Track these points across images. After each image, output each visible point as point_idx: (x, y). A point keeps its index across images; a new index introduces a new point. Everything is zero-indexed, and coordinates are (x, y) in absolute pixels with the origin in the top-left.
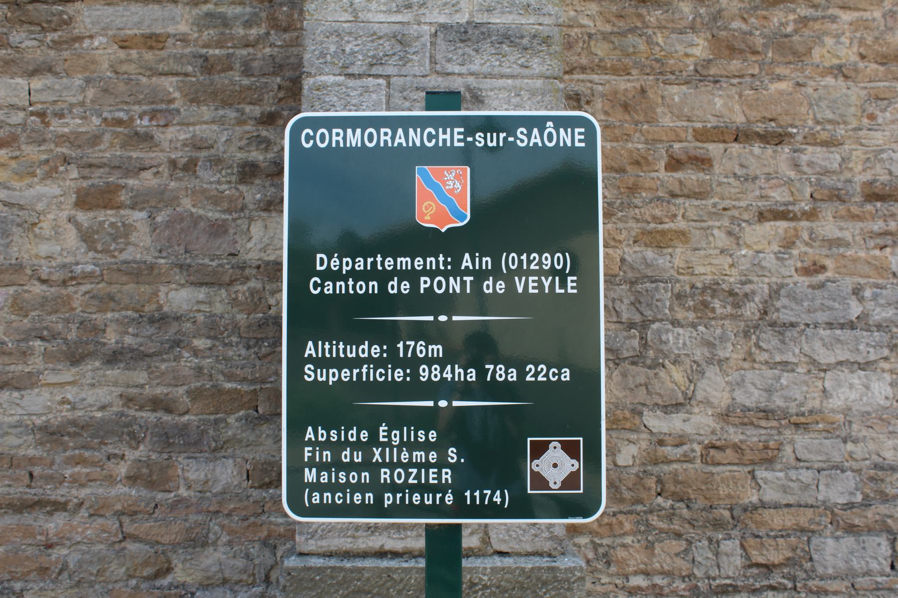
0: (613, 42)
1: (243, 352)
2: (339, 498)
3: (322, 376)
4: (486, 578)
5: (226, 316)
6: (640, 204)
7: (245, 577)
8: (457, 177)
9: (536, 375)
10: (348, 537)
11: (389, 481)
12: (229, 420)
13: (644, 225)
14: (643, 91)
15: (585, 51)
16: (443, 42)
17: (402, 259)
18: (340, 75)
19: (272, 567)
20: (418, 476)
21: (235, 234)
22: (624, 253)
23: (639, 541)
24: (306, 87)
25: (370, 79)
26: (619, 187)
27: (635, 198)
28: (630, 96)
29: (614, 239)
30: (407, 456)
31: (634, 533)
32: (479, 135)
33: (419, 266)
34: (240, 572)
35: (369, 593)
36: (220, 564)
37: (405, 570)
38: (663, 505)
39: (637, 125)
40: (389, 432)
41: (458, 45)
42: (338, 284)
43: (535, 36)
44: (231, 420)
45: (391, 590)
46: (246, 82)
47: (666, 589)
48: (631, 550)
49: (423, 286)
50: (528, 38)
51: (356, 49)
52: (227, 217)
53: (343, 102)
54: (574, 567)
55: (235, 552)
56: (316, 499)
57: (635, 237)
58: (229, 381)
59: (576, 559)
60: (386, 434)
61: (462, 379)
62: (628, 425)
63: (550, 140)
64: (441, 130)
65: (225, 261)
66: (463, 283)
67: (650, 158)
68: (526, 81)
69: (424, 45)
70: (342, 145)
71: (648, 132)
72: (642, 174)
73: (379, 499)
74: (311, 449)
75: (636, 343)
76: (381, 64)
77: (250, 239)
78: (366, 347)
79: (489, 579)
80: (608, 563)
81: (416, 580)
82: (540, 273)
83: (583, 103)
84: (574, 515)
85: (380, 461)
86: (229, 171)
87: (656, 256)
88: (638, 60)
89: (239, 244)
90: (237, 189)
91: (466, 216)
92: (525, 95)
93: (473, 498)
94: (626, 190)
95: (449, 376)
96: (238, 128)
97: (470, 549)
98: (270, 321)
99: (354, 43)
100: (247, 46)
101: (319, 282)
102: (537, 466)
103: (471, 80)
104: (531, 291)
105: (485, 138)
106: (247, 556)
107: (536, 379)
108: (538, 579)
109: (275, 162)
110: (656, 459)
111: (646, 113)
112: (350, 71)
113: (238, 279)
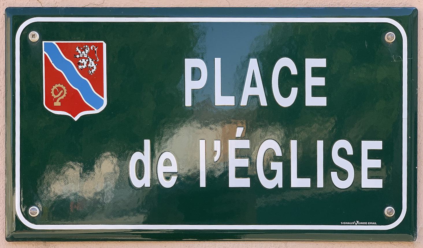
8: (91, 54)
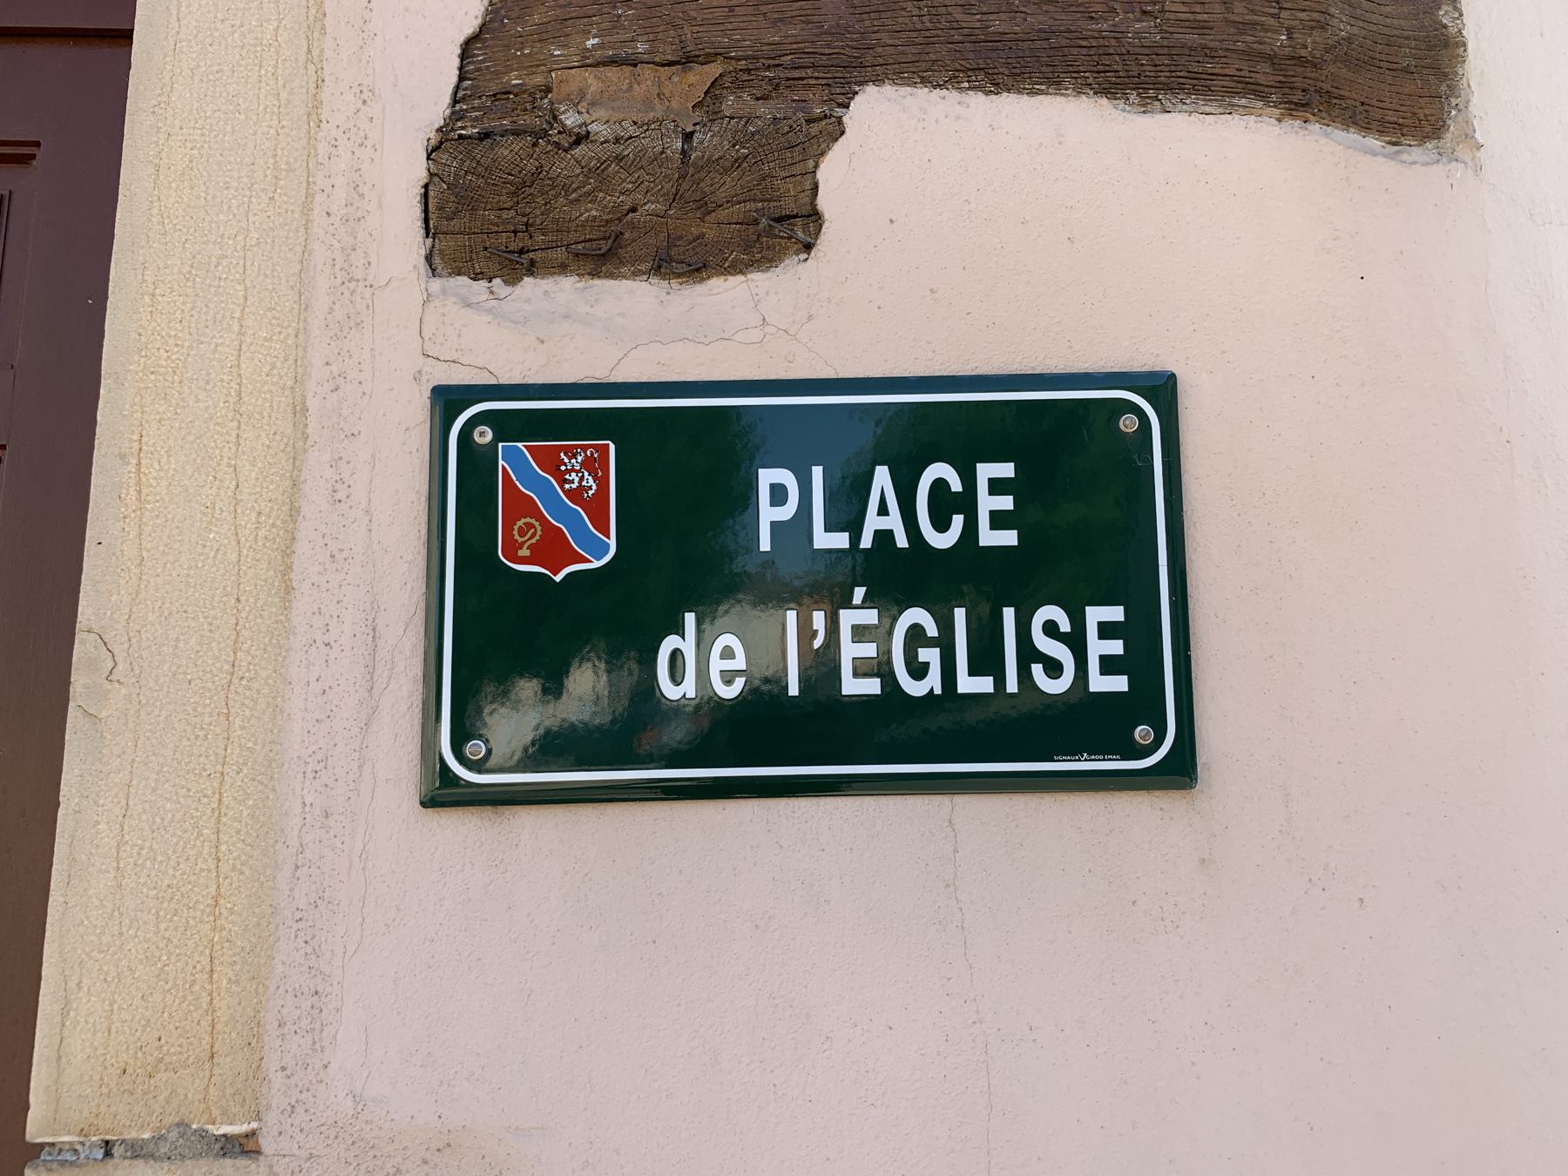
8: (588, 464)
49: (768, 515)
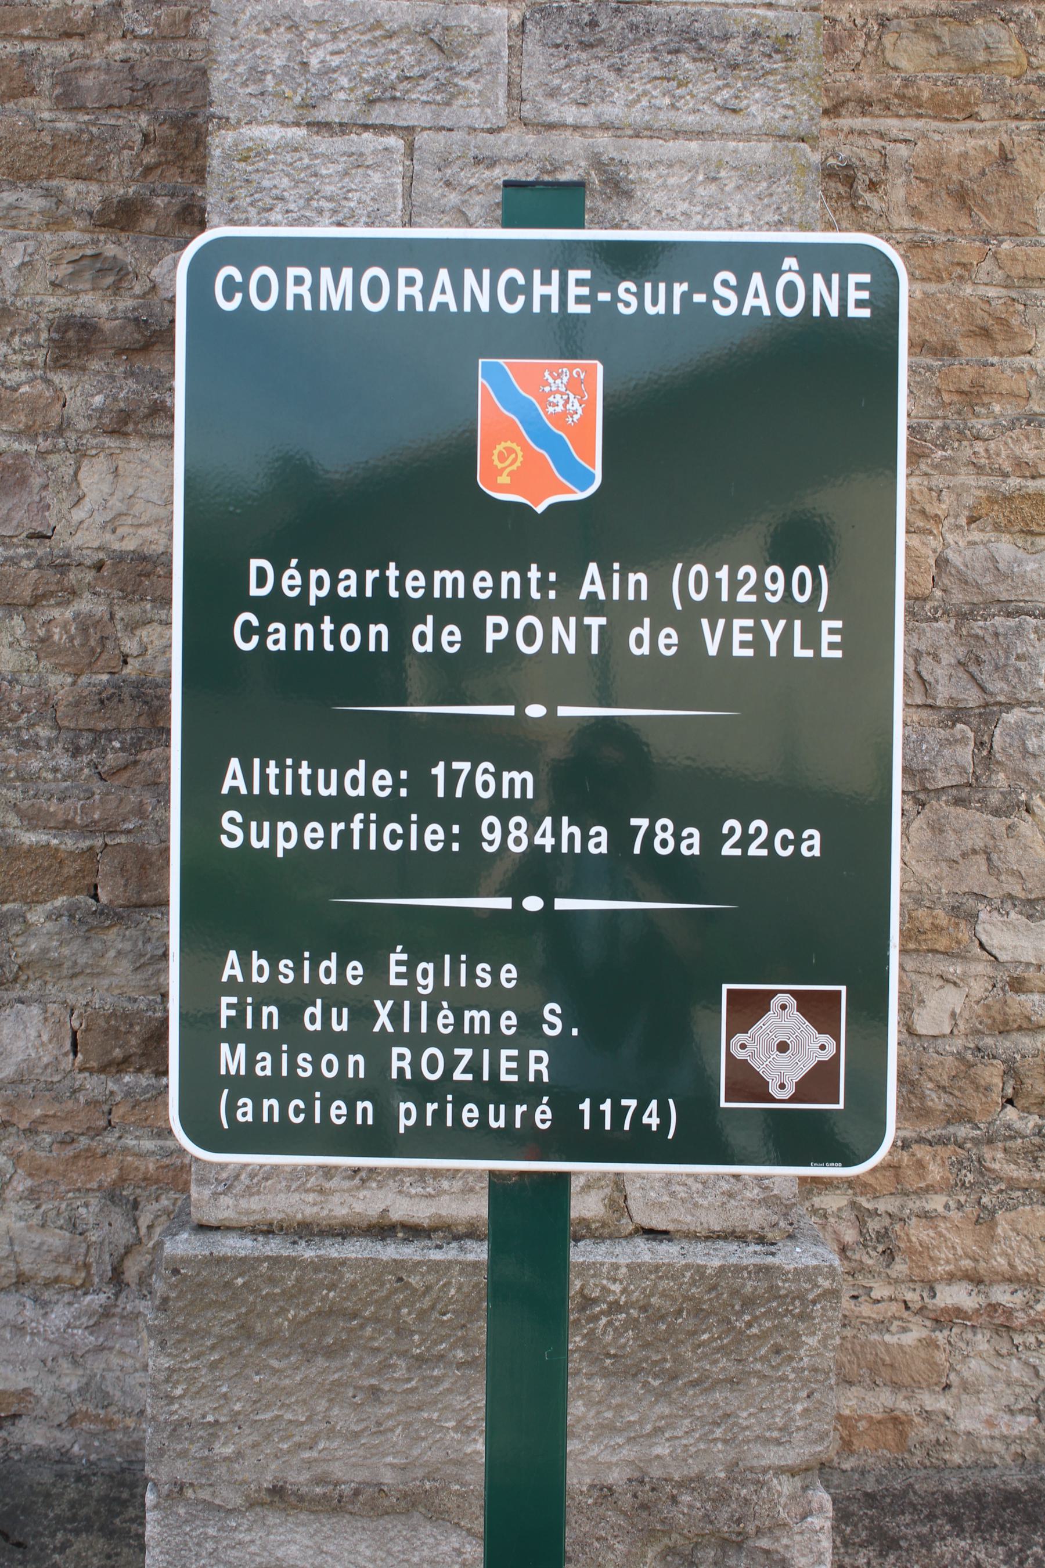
0: (937, 38)
1: (64, 762)
2: (297, 1111)
3: (260, 838)
4: (616, 1288)
5: (25, 678)
6: (987, 432)
7: (66, 1271)
8: (573, 385)
9: (745, 842)
10: (307, 1191)
11: (408, 1076)
12: (32, 917)
13: (996, 480)
14: (1005, 158)
15: (871, 61)
16: (539, 48)
17: (446, 573)
18: (297, 124)
19: (128, 1250)
20: (474, 1067)
21: (45, 487)
22: (946, 545)
23: (960, 1206)
24: (217, 152)
25: (365, 135)
26: (939, 391)
27: (977, 416)
28: (974, 172)
29: (923, 512)
30: (451, 1020)
31: (948, 1188)
32: (626, 288)
33: (483, 590)
34: (55, 1260)
35: (355, 1316)
36: (11, 1243)
37: (435, 1267)
38: (1018, 1125)
39: (986, 242)
40: (411, 965)
41: (574, 56)
42: (299, 628)
43: (756, 35)
44: (36, 916)
45: (405, 1311)
46: (66, 123)
47: (1020, 1314)
48: (942, 1226)
49: (491, 637)
50: (740, 40)
51: (335, 61)
52: (26, 446)
53: (303, 189)
54: (816, 1268)
55: (45, 1213)
56: (245, 1112)
57: (971, 509)
58: (32, 828)
59: (820, 1250)
60: (403, 969)
61: (578, 849)
62: (942, 944)
63: (790, 302)
64: (537, 274)
65: (21, 551)
66: (584, 633)
67: (1015, 321)
68: (732, 144)
69: (495, 54)
70: (308, 306)
71: (1014, 259)
72: (995, 360)
73: (386, 1115)
74: (234, 1000)
75: (966, 754)
76: (394, 99)
77: (80, 499)
78: (361, 773)
79: (624, 1291)
80: (889, 1255)
81: (459, 1289)
82: (760, 610)
83: (860, 187)
84: (824, 1159)
85: (390, 1029)
86: (28, 338)
87: (1021, 554)
88: (996, 82)
89: (54, 511)
90: (48, 382)
91: (592, 477)
92: (730, 179)
93: (597, 1116)
94: (955, 398)
95: (548, 842)
96: (48, 236)
97: (583, 1221)
98: (126, 691)
99: (330, 47)
100: (68, 35)
101: (255, 622)
102: (743, 1046)
103: (603, 141)
104: (737, 652)
105: (640, 295)
106: (73, 1225)
107: (745, 851)
108: (735, 1293)
109: (136, 320)
110: (1006, 1023)
111: (1010, 213)
112: (320, 115)
113: (52, 594)
